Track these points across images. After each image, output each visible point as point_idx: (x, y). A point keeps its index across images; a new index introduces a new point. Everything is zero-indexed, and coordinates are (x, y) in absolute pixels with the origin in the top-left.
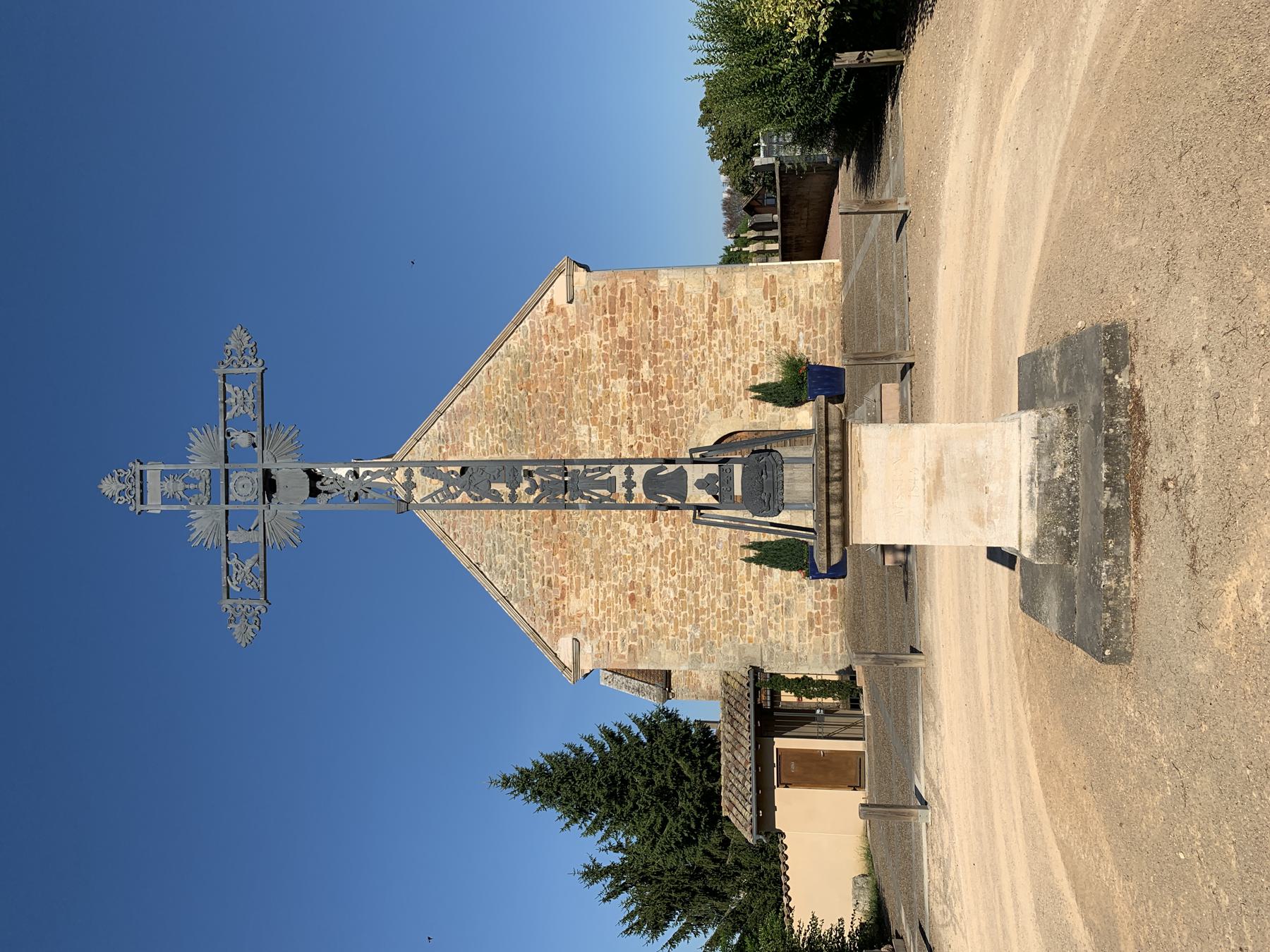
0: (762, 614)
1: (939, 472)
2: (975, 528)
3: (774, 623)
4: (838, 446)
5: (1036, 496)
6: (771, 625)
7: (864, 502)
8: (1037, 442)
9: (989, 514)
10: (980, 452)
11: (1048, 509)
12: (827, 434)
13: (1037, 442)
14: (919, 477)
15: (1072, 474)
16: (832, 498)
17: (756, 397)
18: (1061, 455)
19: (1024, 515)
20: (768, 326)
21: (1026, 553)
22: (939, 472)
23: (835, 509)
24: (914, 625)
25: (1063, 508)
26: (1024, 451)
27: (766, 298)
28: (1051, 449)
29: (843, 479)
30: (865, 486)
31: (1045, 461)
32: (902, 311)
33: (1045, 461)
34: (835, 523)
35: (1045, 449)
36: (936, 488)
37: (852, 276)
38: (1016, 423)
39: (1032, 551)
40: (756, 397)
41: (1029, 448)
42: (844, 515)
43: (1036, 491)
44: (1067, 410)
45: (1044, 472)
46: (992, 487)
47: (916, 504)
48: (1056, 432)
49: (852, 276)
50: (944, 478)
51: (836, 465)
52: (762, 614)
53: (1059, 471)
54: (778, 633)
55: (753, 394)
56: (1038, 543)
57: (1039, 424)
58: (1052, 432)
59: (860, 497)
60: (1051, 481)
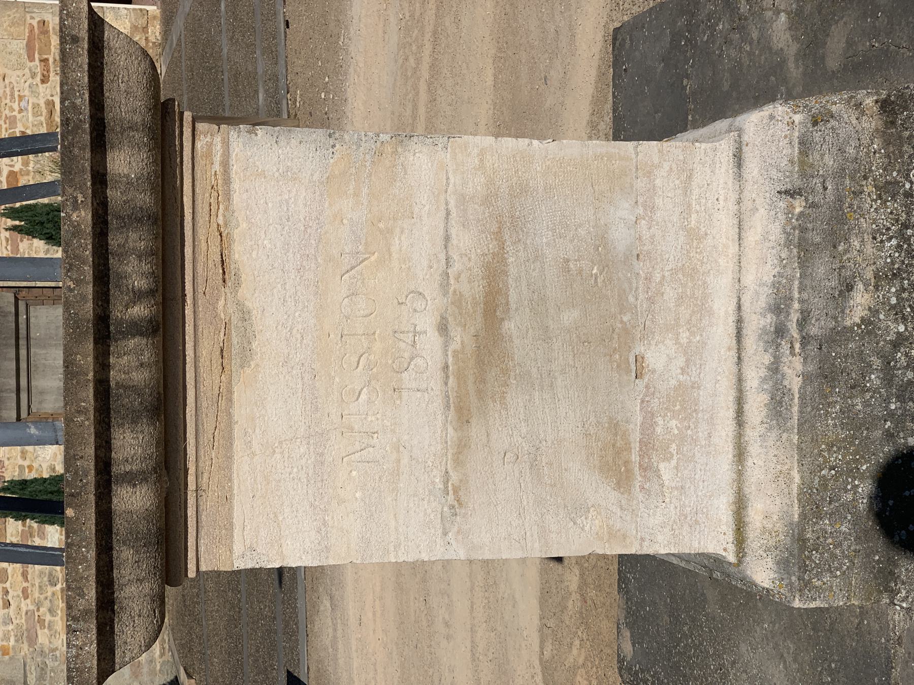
0: (27, 605)
1: (493, 307)
2: (604, 495)
3: (48, 618)
4: (145, 199)
5: (795, 383)
6: (41, 622)
7: (240, 412)
8: (799, 206)
9: (647, 445)
10: (620, 236)
11: (831, 426)
12: (99, 143)
13: (799, 206)
14: (427, 322)
15: (897, 311)
16: (122, 402)
17: (14, 228)
18: (866, 251)
19: (754, 449)
20: (36, 106)
21: (762, 573)
22: (493, 307)
23: (132, 445)
24: (295, 632)
25: (870, 423)
26: (752, 237)
27: (31, 58)
28: (837, 228)
29: (166, 329)
30: (246, 354)
31: (821, 268)
32: (273, 54)
33: (821, 268)
34: (134, 501)
35: (817, 232)
36: (485, 353)
37: (179, 23)
38: (725, 147)
39: (783, 565)
40: (14, 228)
41: (767, 227)
42: (169, 466)
43: (794, 371)
44: (885, 105)
45: (817, 303)
46: (660, 356)
47: (421, 420)
48: (853, 172)
49: (179, 23)
50: (510, 326)
51: (135, 273)
52: (27, 605)
53: (861, 301)
54: (53, 634)
55: (10, 223)
56: (801, 540)
57: (805, 145)
58: (840, 173)
59: (225, 395)
60: (838, 335)
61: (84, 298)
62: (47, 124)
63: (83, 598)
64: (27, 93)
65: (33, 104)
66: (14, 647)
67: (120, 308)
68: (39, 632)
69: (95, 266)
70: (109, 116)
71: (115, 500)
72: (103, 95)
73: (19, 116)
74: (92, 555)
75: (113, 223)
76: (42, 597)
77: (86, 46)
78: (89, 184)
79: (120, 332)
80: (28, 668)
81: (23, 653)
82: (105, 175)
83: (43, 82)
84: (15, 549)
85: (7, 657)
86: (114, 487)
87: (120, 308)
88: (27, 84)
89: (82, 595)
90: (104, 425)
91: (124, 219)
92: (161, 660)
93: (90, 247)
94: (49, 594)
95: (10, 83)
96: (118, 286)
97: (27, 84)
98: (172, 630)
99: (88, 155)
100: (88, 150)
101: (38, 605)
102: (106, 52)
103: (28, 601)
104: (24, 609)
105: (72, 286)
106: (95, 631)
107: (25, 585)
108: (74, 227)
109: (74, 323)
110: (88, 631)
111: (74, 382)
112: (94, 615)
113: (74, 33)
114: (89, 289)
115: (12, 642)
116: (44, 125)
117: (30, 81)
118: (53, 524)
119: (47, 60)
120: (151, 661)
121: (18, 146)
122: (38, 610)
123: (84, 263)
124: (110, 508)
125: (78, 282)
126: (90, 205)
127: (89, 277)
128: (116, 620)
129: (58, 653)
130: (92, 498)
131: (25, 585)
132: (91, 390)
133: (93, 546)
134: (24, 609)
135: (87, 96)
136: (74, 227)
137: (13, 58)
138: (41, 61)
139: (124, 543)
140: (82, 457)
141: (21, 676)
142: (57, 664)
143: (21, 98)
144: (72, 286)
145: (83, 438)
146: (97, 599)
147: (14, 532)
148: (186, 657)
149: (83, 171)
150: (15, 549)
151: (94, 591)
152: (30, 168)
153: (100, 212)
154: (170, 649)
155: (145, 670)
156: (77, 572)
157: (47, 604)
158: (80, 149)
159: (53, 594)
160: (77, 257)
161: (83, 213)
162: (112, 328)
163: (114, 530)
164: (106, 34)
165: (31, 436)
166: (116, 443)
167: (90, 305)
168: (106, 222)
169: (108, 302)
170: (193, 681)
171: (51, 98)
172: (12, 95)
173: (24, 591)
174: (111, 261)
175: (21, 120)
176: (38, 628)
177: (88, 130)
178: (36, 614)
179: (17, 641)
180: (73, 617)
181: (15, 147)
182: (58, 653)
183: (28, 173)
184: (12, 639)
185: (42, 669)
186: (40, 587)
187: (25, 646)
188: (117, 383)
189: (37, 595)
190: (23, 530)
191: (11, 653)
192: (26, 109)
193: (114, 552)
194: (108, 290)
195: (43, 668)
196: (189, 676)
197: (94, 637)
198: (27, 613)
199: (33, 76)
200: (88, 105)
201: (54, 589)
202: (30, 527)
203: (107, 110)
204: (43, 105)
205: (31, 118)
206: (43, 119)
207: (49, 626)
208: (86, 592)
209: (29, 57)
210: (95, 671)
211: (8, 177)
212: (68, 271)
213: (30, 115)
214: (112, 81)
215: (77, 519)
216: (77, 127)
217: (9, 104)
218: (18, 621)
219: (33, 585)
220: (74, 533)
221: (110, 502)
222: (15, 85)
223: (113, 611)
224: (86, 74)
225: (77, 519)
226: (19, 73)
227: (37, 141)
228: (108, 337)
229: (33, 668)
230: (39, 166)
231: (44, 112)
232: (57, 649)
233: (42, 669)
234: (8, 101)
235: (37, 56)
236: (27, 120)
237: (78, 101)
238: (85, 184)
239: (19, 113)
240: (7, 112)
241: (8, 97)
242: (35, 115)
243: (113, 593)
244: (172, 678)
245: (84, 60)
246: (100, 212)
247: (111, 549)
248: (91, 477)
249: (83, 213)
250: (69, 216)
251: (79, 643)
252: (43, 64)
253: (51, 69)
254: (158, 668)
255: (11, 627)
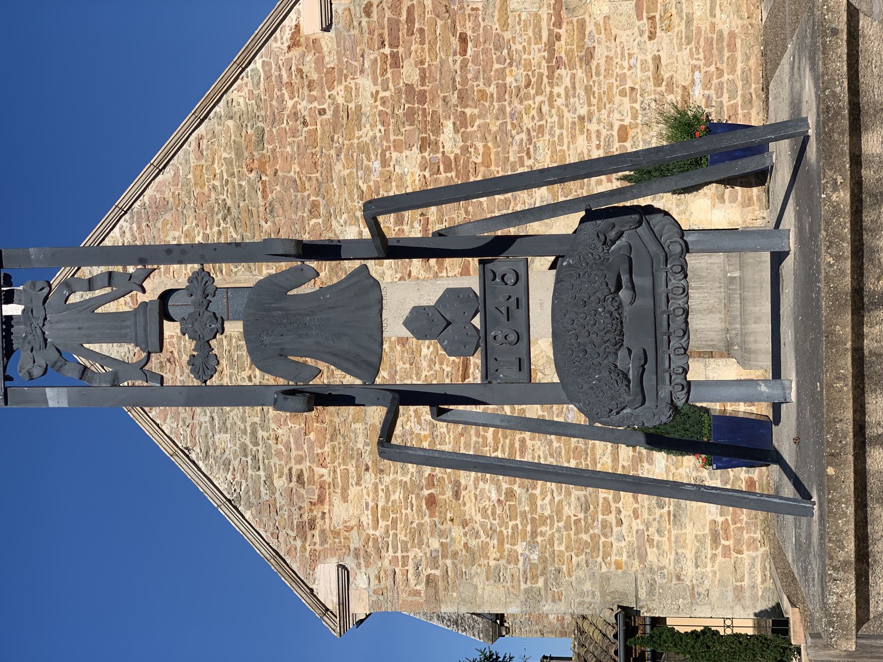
0: (637, 525)
3: (656, 537)
6: (650, 541)
27: (639, 17)
52: (637, 525)
61: (842, 272)
62: (654, 78)
63: (843, 550)
64: (636, 50)
65: (641, 60)
66: (626, 563)
67: (873, 280)
68: (649, 550)
69: (853, 241)
70: (863, 100)
71: (869, 461)
72: (858, 81)
73: (628, 73)
74: (851, 511)
75: (867, 200)
76: (651, 518)
77: (845, 37)
78: (848, 166)
79: (872, 303)
80: (639, 582)
81: (634, 569)
82: (860, 156)
83: (650, 38)
84: (770, 499)
85: (620, 571)
86: (868, 449)
87: (873, 280)
88: (636, 42)
89: (842, 548)
90: (859, 390)
91: (876, 196)
92: (762, 586)
93: (848, 225)
94: (657, 516)
95: (621, 42)
96: (871, 260)
97: (636, 42)
98: (774, 558)
99: (847, 139)
100: (847, 134)
101: (648, 525)
102: (861, 40)
103: (639, 521)
104: (635, 528)
105: (832, 262)
106: (853, 582)
107: (636, 506)
108: (834, 207)
109: (834, 296)
110: (847, 581)
111: (834, 351)
112: (853, 566)
113: (834, 26)
114: (848, 264)
115: (625, 558)
116: (652, 79)
117: (639, 38)
118: (660, 451)
119: (654, 17)
120: (753, 587)
121: (771, 133)
122: (647, 530)
123: (843, 240)
124: (865, 468)
125: (837, 258)
126: (848, 185)
127: (848, 253)
128: (870, 572)
129: (665, 571)
130: (851, 458)
131: (636, 506)
132: (850, 358)
133: (852, 502)
134: (635, 528)
135: (846, 84)
136: (834, 207)
137: (624, 18)
138: (648, 19)
139: (877, 500)
140: (841, 420)
141: (633, 589)
142: (665, 581)
143: (630, 55)
144: (832, 262)
145: (842, 402)
146: (856, 552)
147: (626, 457)
148: (790, 586)
149: (843, 154)
150: (770, 499)
151: (853, 544)
152: (639, 121)
153: (856, 191)
154: (771, 577)
155: (747, 594)
156: (837, 526)
157: (655, 524)
158: (839, 134)
159: (661, 516)
160: (836, 235)
161: (842, 194)
162: (866, 299)
163: (869, 489)
164: (861, 22)
165: (762, 393)
166: (870, 407)
167: (848, 279)
168: (861, 201)
169: (862, 275)
170: (797, 609)
171: (657, 54)
172: (623, 54)
173: (635, 511)
174: (865, 237)
175: (630, 77)
176: (648, 547)
177: (847, 116)
178: (646, 533)
179: (629, 557)
180: (833, 567)
181: (769, 134)
182: (665, 571)
183: (636, 126)
184: (625, 554)
185: (652, 585)
186: (649, 509)
187: (636, 562)
188: (870, 351)
189: (646, 516)
190: (633, 456)
191: (624, 568)
192: (635, 66)
193: (869, 509)
194: (863, 264)
195: (652, 584)
196: (793, 605)
197: (853, 587)
198: (637, 532)
199: (641, 33)
200: (846, 92)
201: (662, 511)
202: (639, 453)
203: (861, 95)
204: (650, 61)
205: (639, 74)
206: (650, 74)
207: (658, 546)
208: (846, 545)
209: (637, 16)
210: (854, 618)
211: (618, 131)
212: (828, 248)
213: (639, 70)
214: (866, 67)
215: (837, 477)
216: (837, 114)
217: (620, 62)
218: (629, 539)
219: (643, 507)
220: (834, 490)
221: (865, 462)
222: (625, 44)
223: (868, 564)
224: (845, 63)
225: (837, 477)
226: (629, 32)
227: (789, 127)
228: (863, 308)
229: (643, 584)
230: (646, 118)
231: (652, 67)
232: (664, 567)
233: (652, 585)
234: (618, 60)
235: (645, 14)
236: (636, 76)
237: (838, 89)
238: (844, 166)
239: (629, 70)
240: (618, 70)
241: (619, 56)
242: (644, 70)
243: (868, 547)
244: (774, 604)
245: (843, 50)
246: (856, 191)
247: (866, 506)
248: (850, 439)
249: (842, 194)
250: (829, 197)
251: (839, 591)
252: (650, 21)
253: (658, 26)
254: (760, 594)
255: (623, 544)
